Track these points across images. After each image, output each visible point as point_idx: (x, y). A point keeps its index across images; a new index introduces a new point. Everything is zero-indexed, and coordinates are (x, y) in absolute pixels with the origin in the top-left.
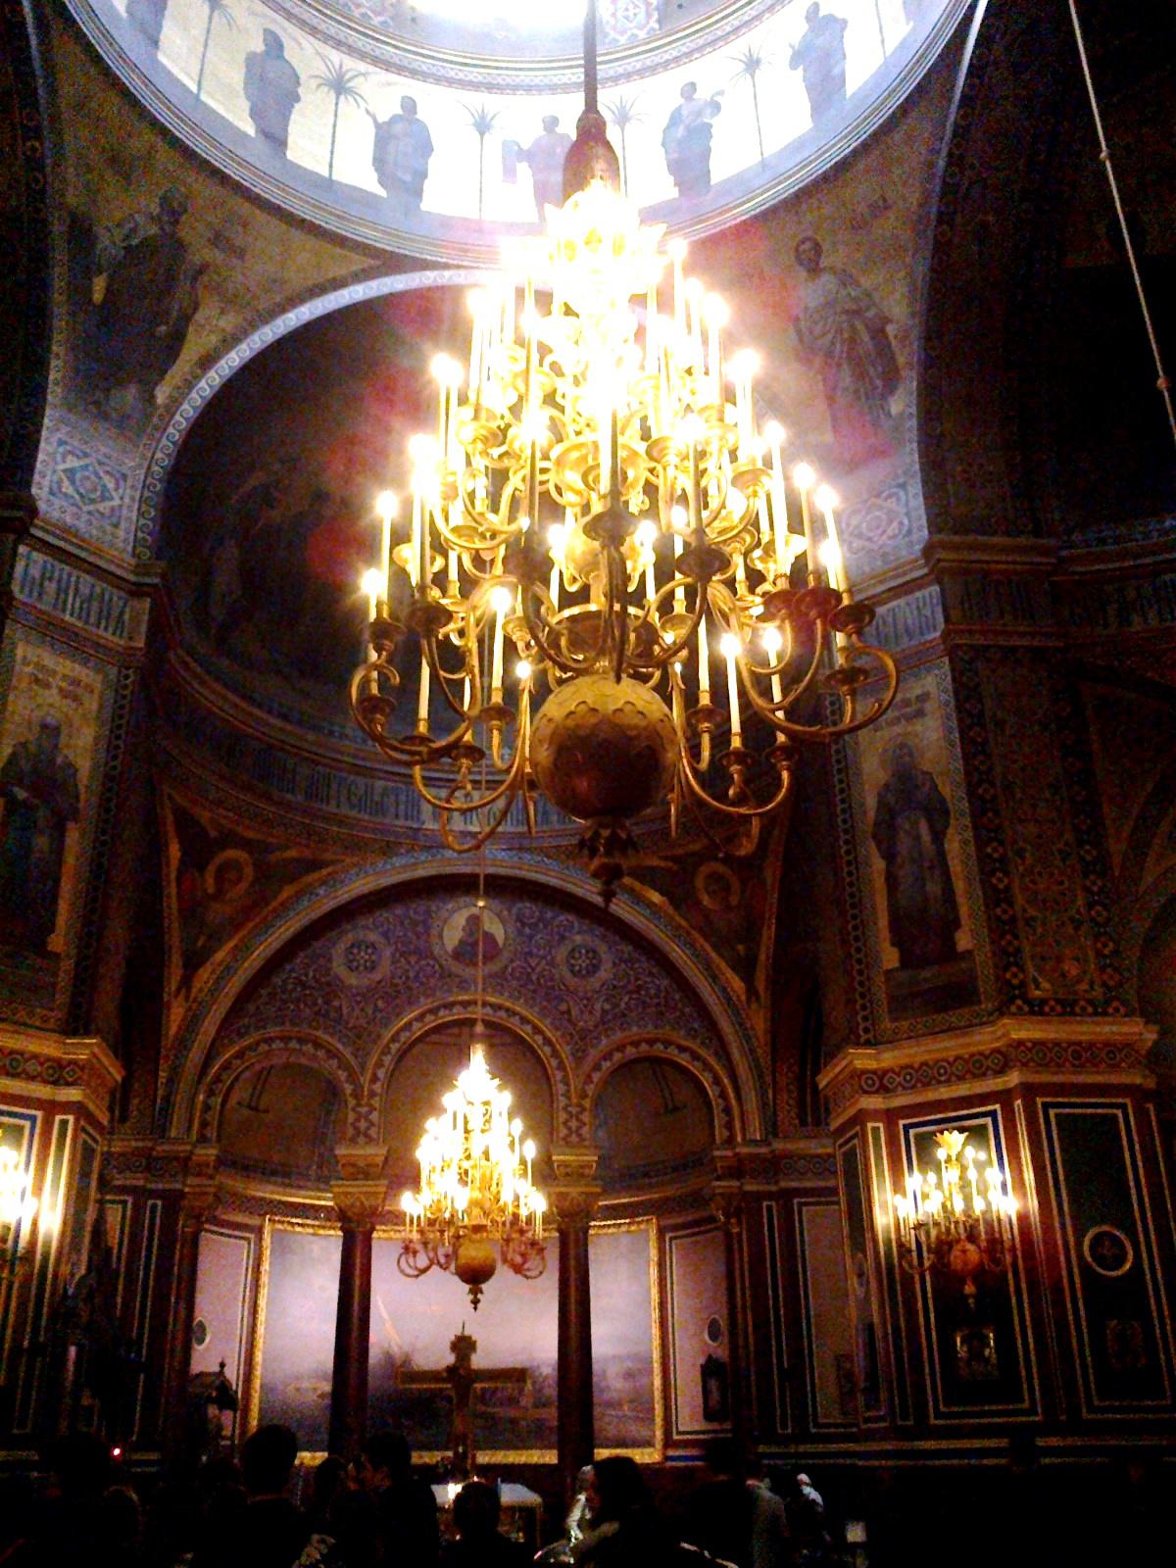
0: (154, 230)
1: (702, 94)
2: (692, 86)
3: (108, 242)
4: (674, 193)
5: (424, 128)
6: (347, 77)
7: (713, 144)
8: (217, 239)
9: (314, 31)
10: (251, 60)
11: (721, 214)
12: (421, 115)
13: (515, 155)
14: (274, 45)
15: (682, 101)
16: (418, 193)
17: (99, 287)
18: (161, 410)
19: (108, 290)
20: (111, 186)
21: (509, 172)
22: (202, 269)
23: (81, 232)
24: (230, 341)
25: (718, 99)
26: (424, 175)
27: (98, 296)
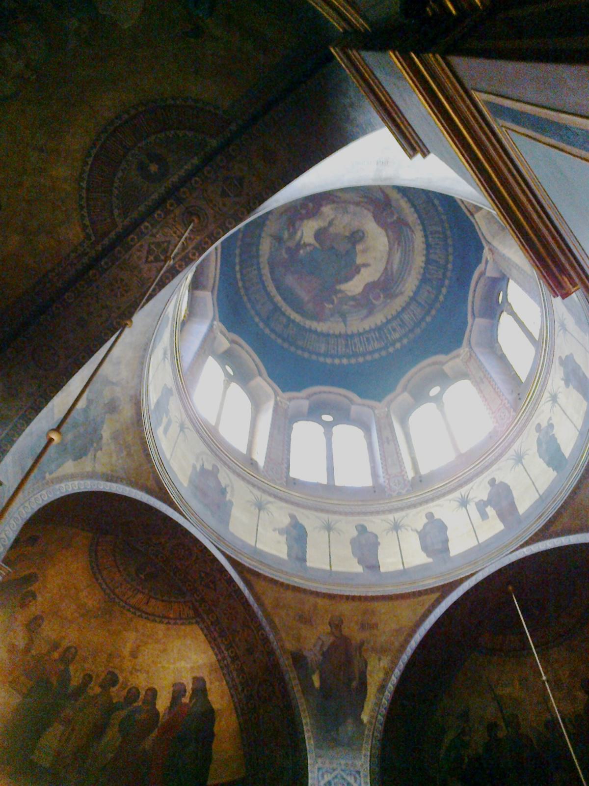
0: (332, 639)
1: (544, 424)
2: (539, 425)
3: (312, 654)
4: (555, 473)
5: (440, 521)
6: (399, 521)
7: (558, 442)
8: (363, 627)
9: (372, 513)
10: (353, 542)
11: (576, 469)
12: (436, 516)
13: (481, 507)
14: (362, 529)
15: (538, 434)
16: (305, 560)
17: (316, 681)
18: (368, 726)
19: (321, 677)
20: (305, 631)
21: (484, 516)
22: (362, 643)
23: (298, 659)
24: (388, 673)
25: (551, 422)
26: (447, 541)
27: (317, 684)
